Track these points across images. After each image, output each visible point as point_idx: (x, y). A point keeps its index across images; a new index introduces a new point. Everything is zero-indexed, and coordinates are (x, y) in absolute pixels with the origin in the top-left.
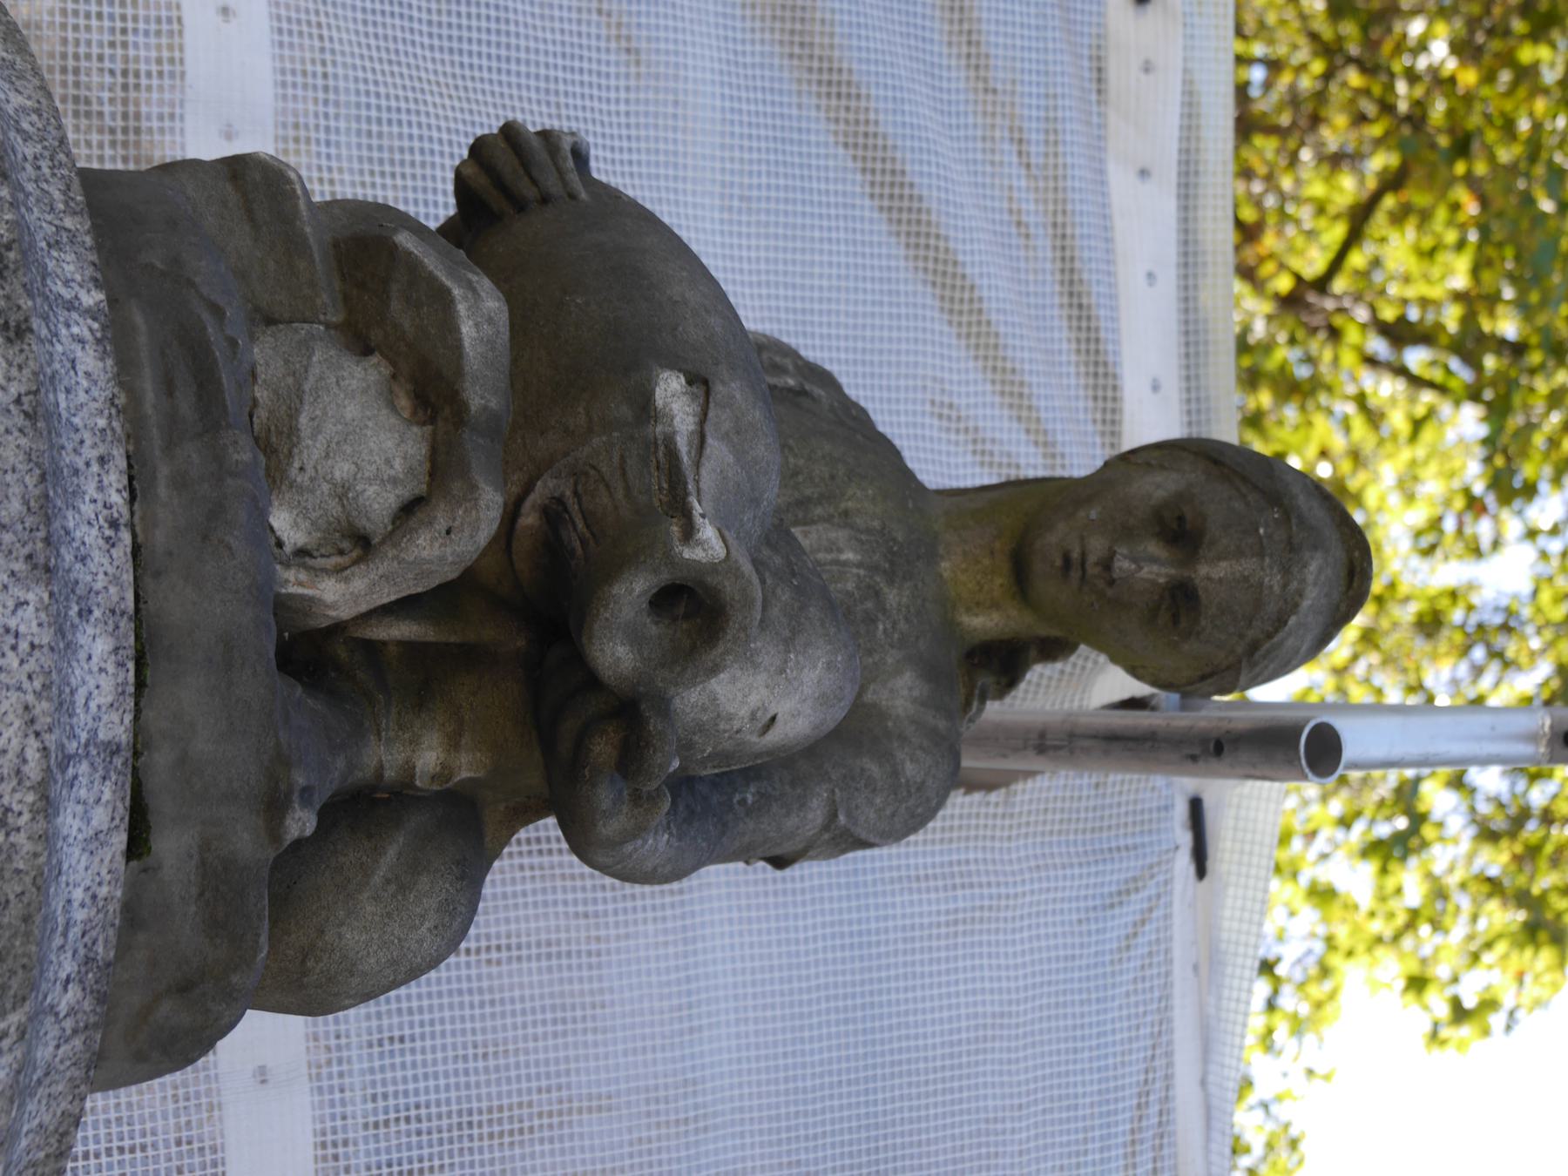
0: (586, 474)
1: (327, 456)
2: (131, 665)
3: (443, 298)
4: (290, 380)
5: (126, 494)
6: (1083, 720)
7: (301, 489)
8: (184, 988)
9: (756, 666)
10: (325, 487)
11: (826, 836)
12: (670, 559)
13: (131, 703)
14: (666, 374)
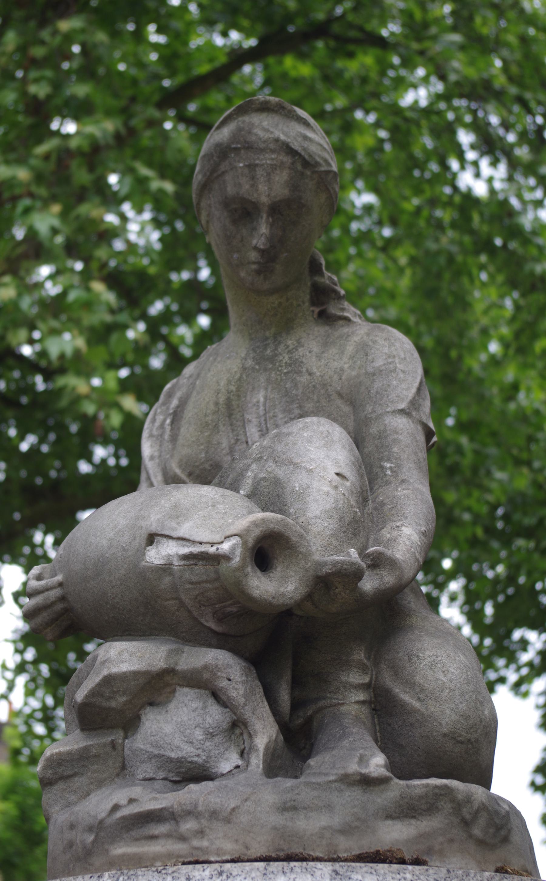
0: (200, 601)
1: (191, 743)
2: (293, 864)
3: (109, 680)
4: (153, 761)
5: (206, 866)
6: (260, 536)
7: (209, 757)
8: (466, 824)
9: (308, 487)
10: (208, 744)
11: (414, 413)
12: (242, 568)
13: (311, 864)
14: (148, 558)
